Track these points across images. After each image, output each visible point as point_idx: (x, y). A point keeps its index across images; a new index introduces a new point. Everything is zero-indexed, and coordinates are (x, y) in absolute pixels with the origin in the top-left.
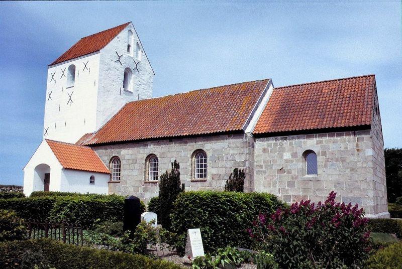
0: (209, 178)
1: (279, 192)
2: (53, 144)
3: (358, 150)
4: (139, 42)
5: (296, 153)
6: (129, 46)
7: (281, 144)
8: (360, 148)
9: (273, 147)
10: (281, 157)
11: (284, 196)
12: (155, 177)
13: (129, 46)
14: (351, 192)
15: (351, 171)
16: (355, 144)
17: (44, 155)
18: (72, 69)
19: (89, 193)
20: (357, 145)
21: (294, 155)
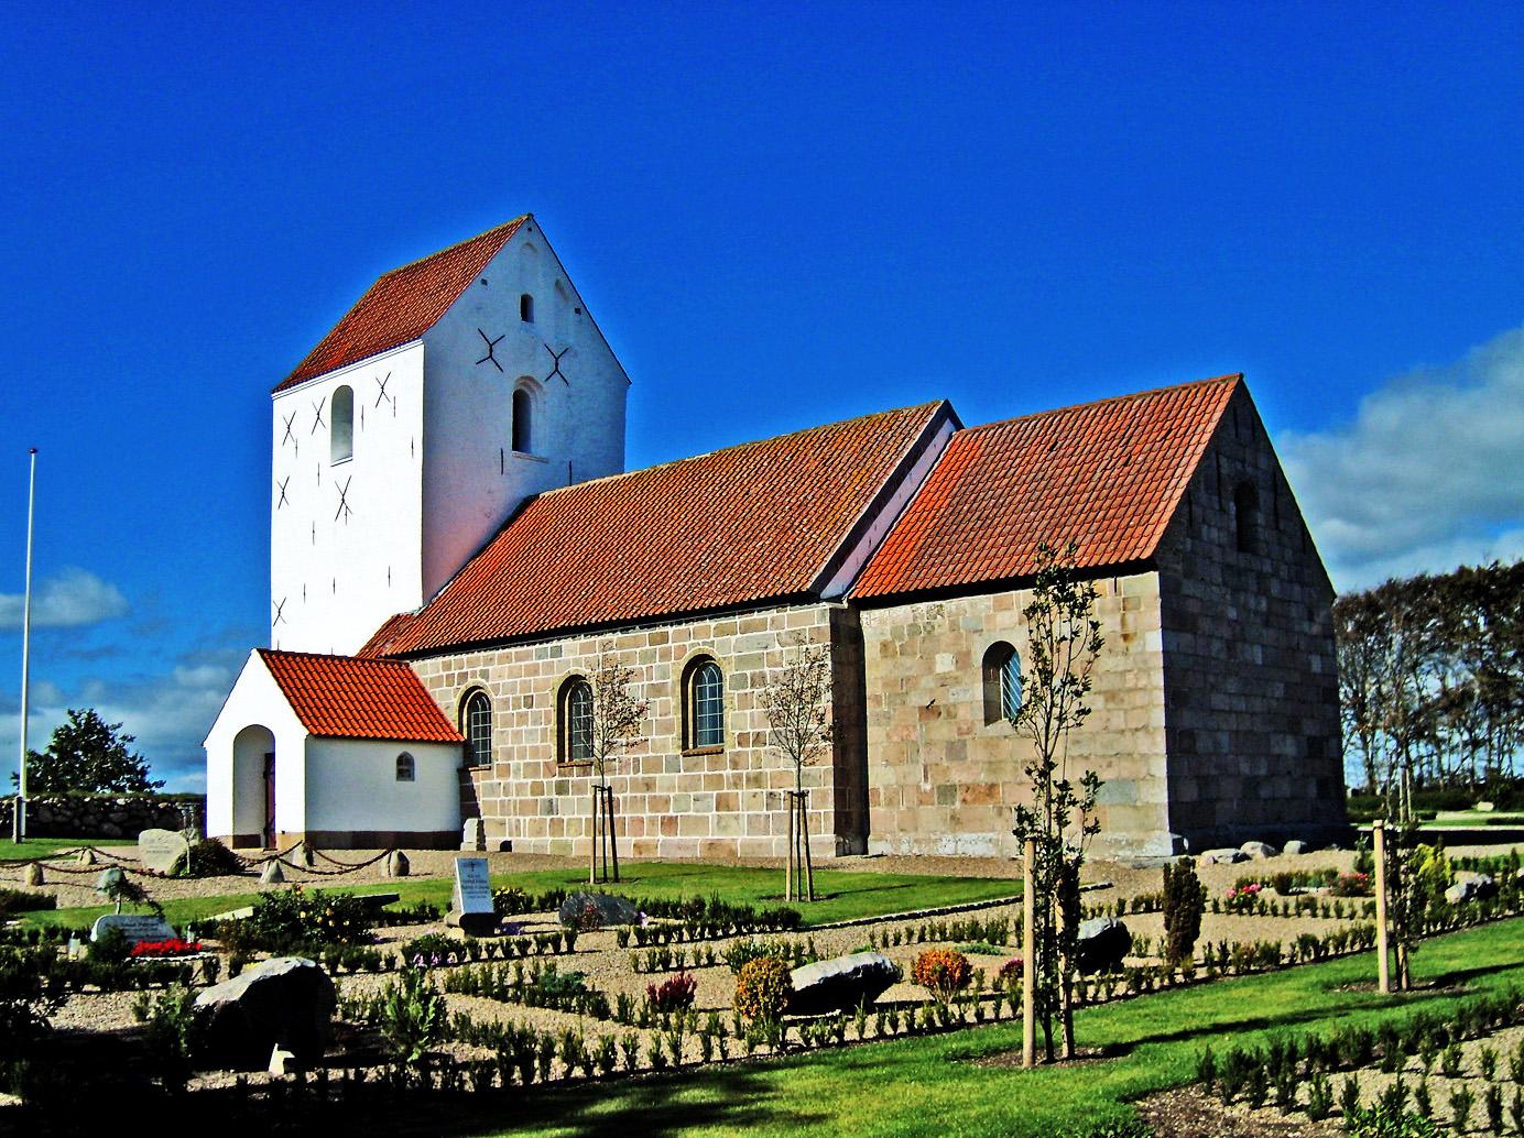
0: (730, 745)
1: (926, 777)
2: (284, 666)
3: (1125, 637)
4: (563, 281)
5: (968, 653)
6: (526, 304)
7: (929, 628)
8: (1130, 629)
9: (906, 638)
10: (930, 670)
11: (939, 787)
12: (484, 735)
13: (526, 304)
14: (1110, 765)
15: (1107, 701)
16: (1119, 618)
17: (257, 698)
18: (343, 403)
19: (587, 983)
20: (1123, 622)
21: (962, 660)
